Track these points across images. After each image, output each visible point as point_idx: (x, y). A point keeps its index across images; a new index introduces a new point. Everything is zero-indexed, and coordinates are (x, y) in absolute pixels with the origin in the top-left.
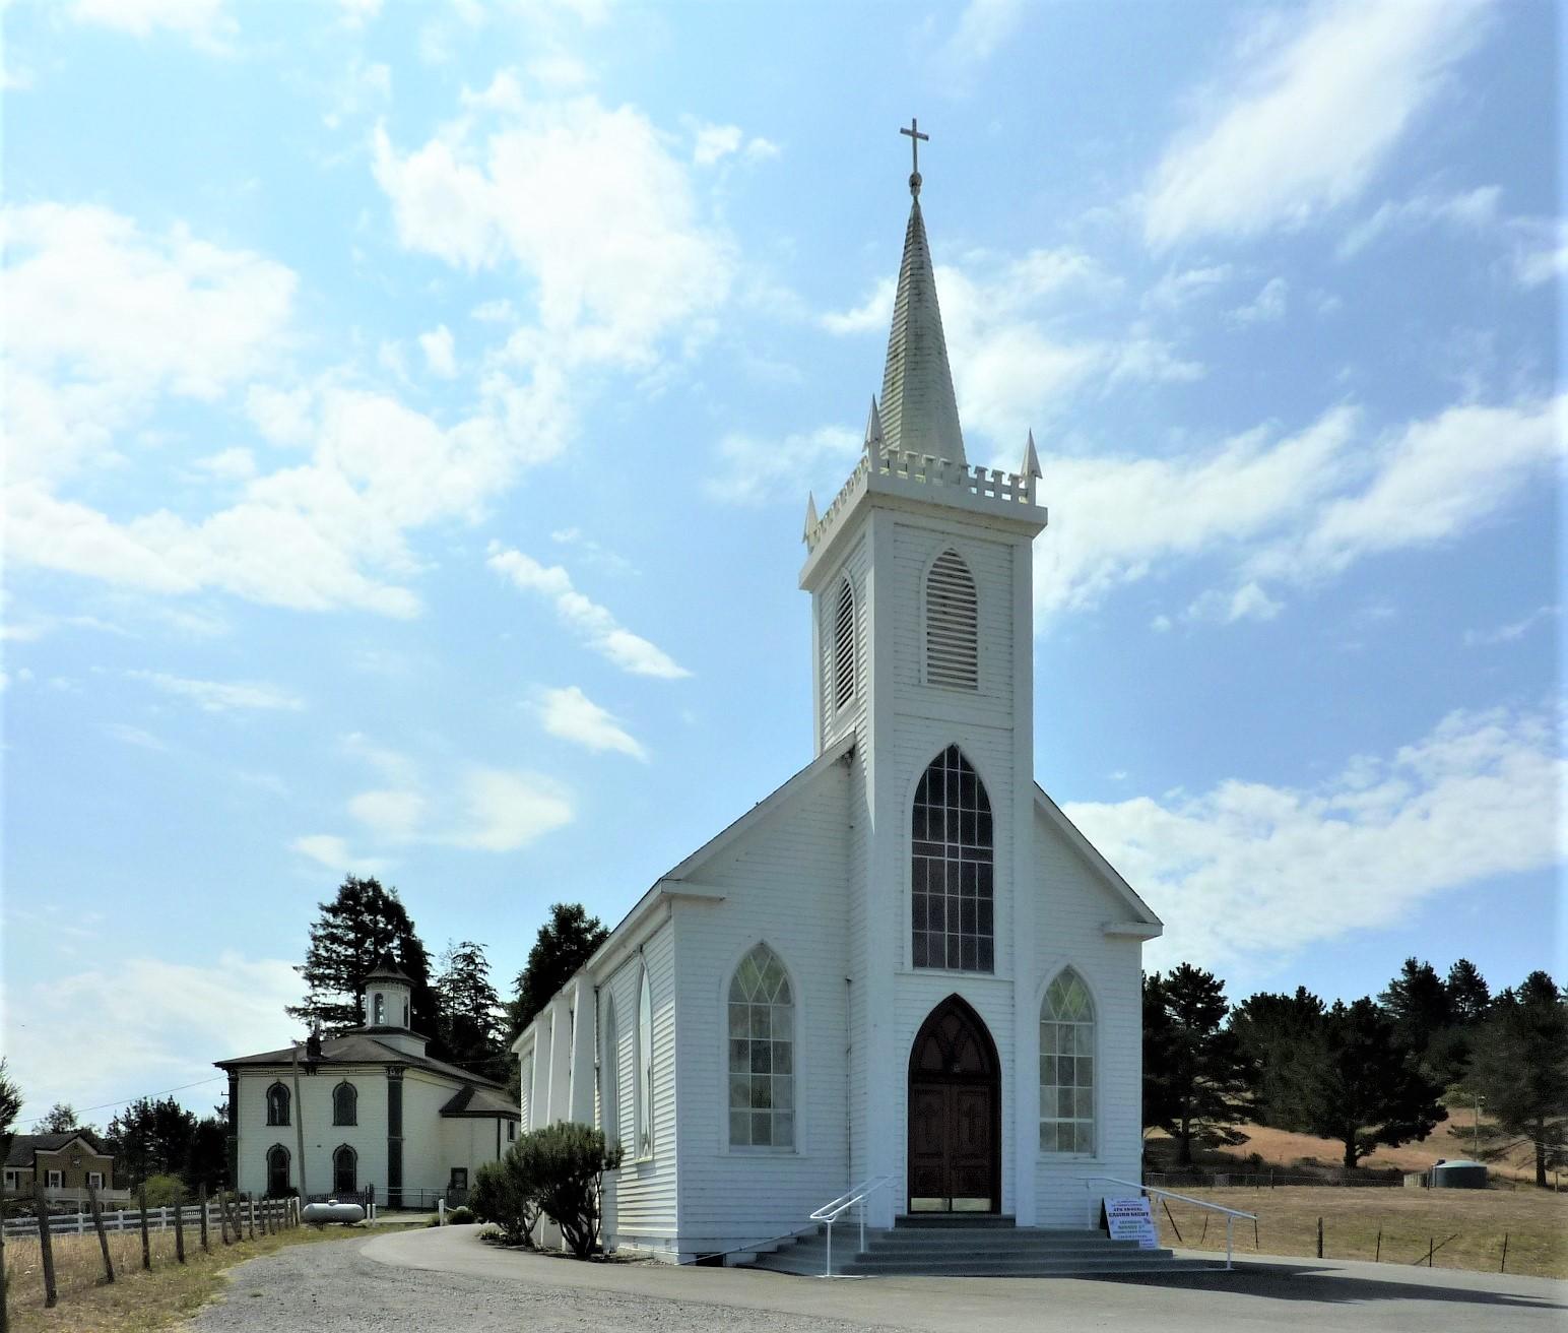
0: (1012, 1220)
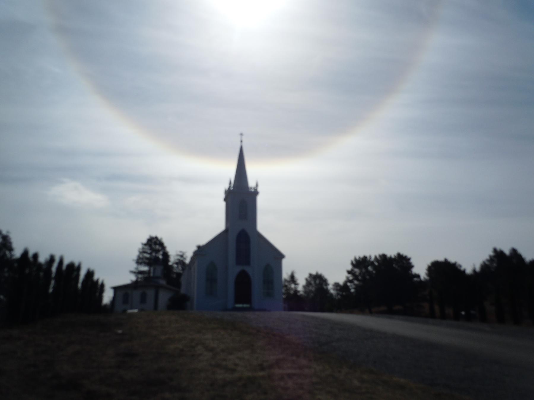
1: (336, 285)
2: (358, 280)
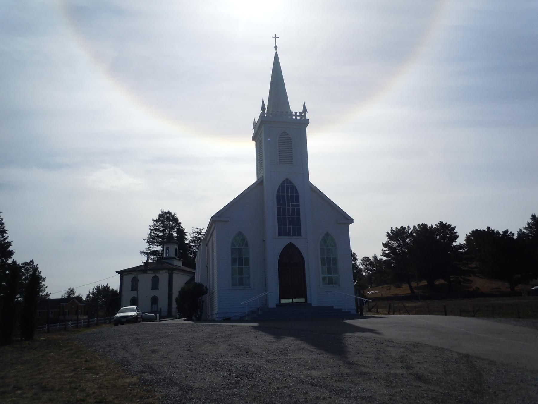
0: (311, 304)
1: (366, 259)
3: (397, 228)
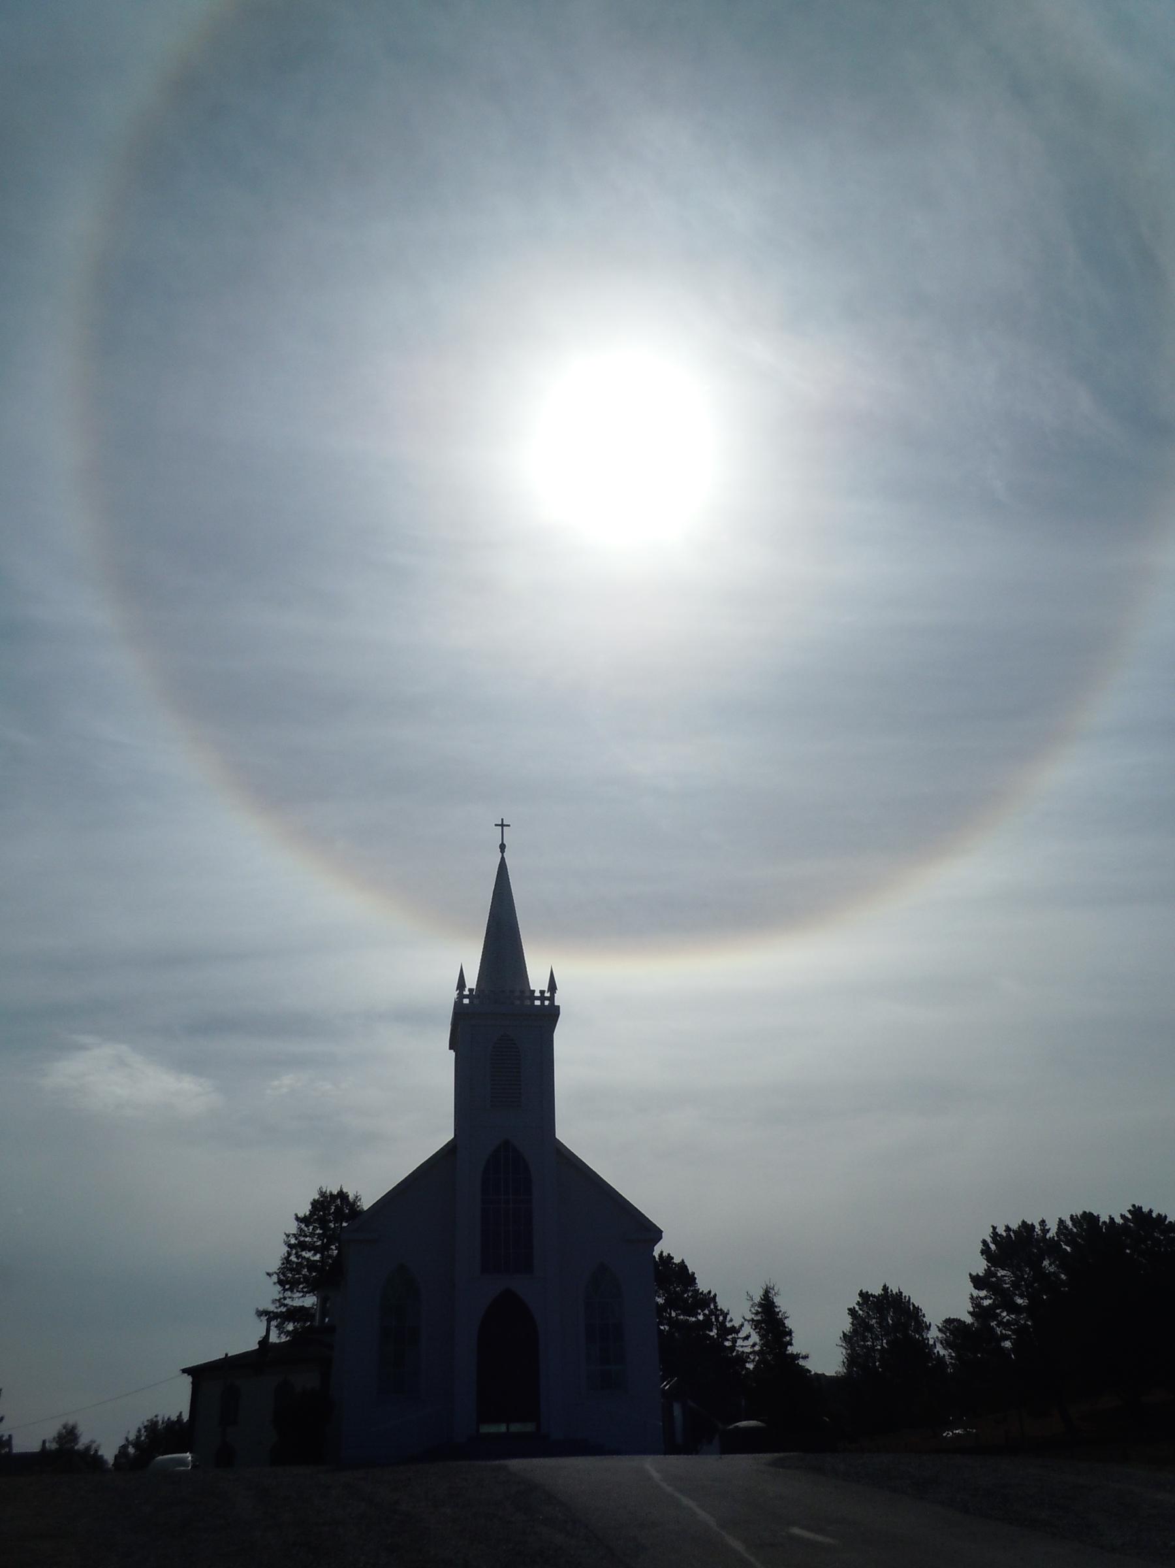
2: (1013, 1308)
3: (1008, 1229)
